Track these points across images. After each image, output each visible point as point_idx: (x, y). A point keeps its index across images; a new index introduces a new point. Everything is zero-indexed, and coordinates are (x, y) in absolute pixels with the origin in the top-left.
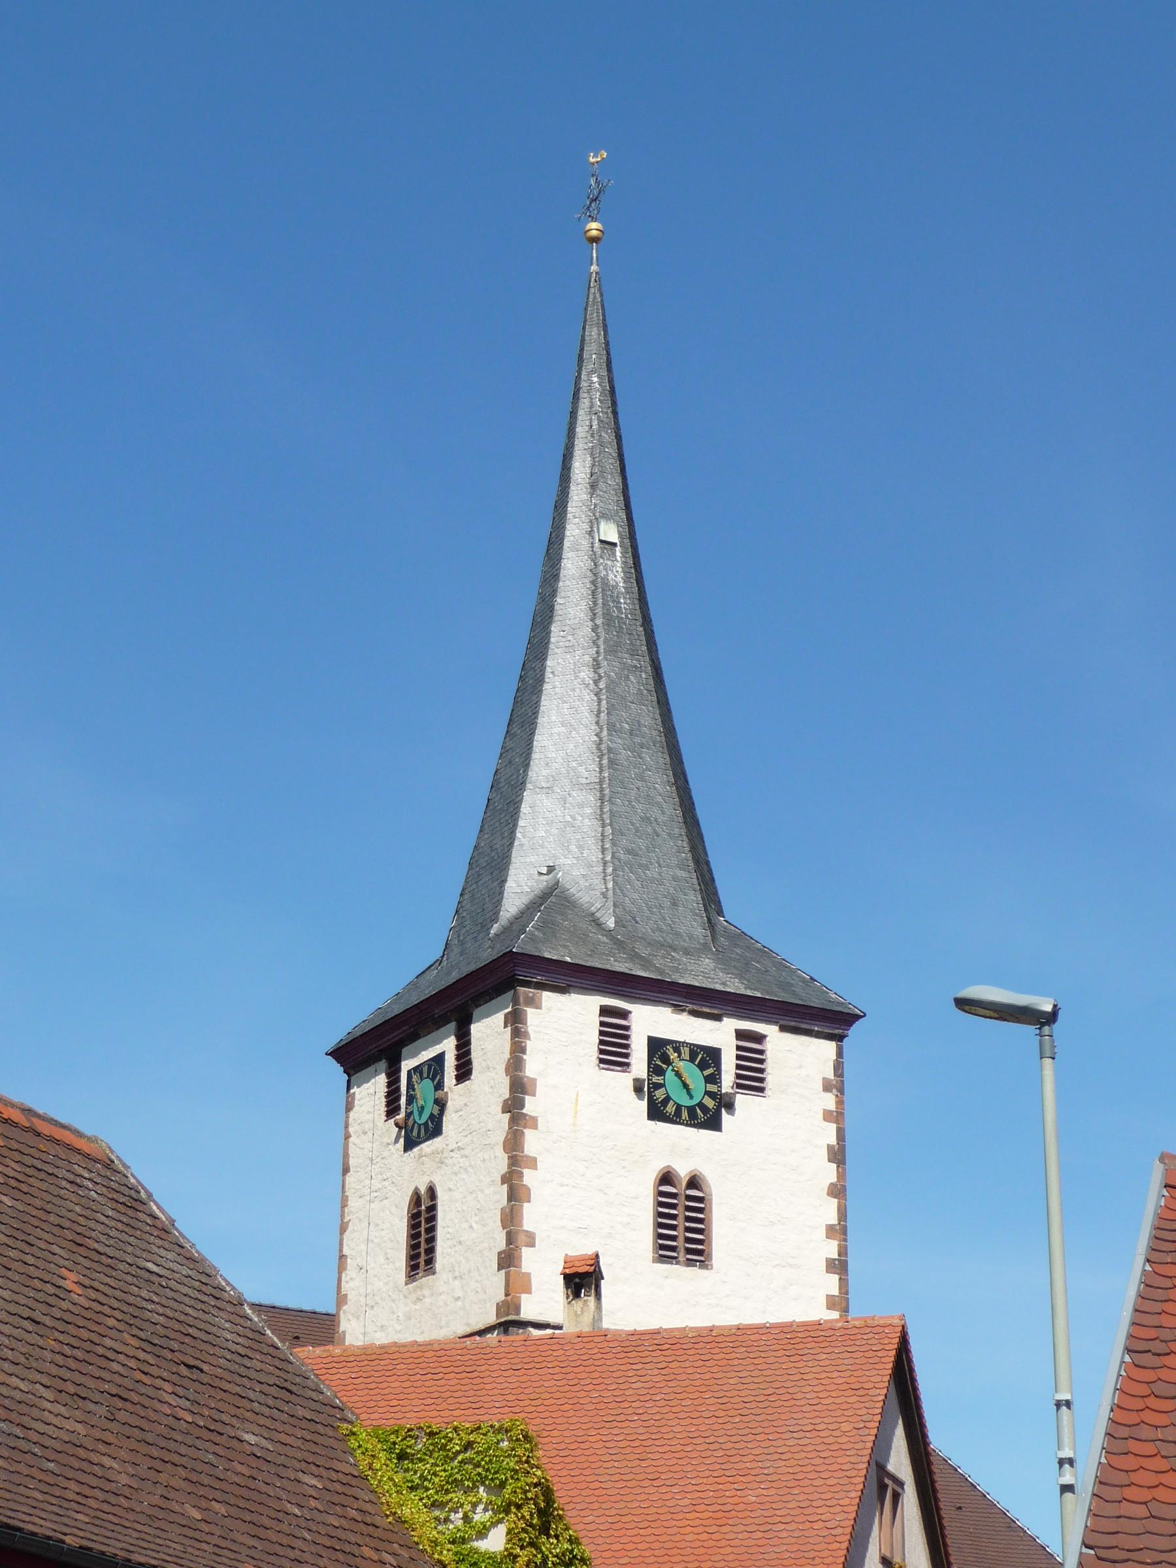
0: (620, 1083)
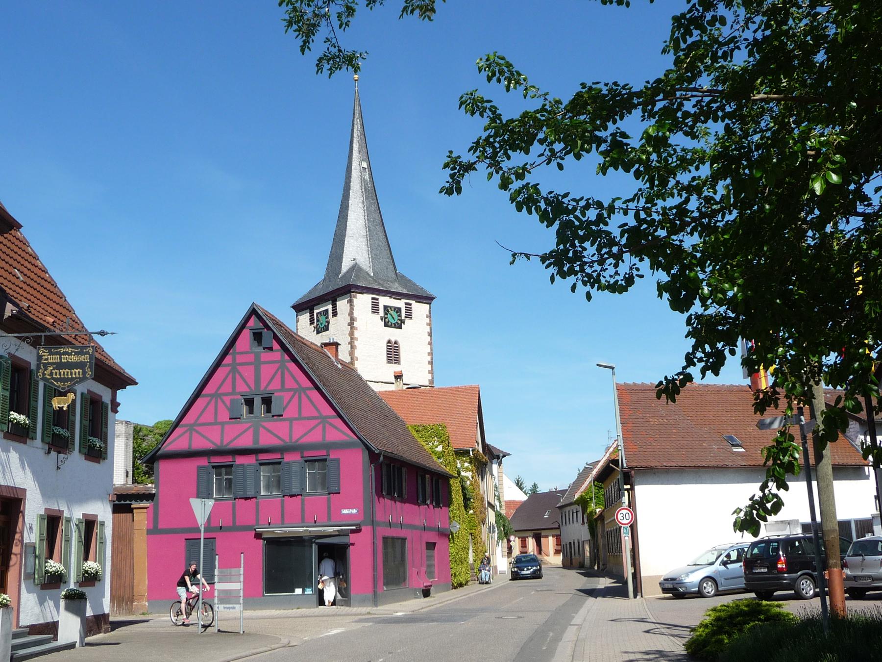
0: (377, 317)
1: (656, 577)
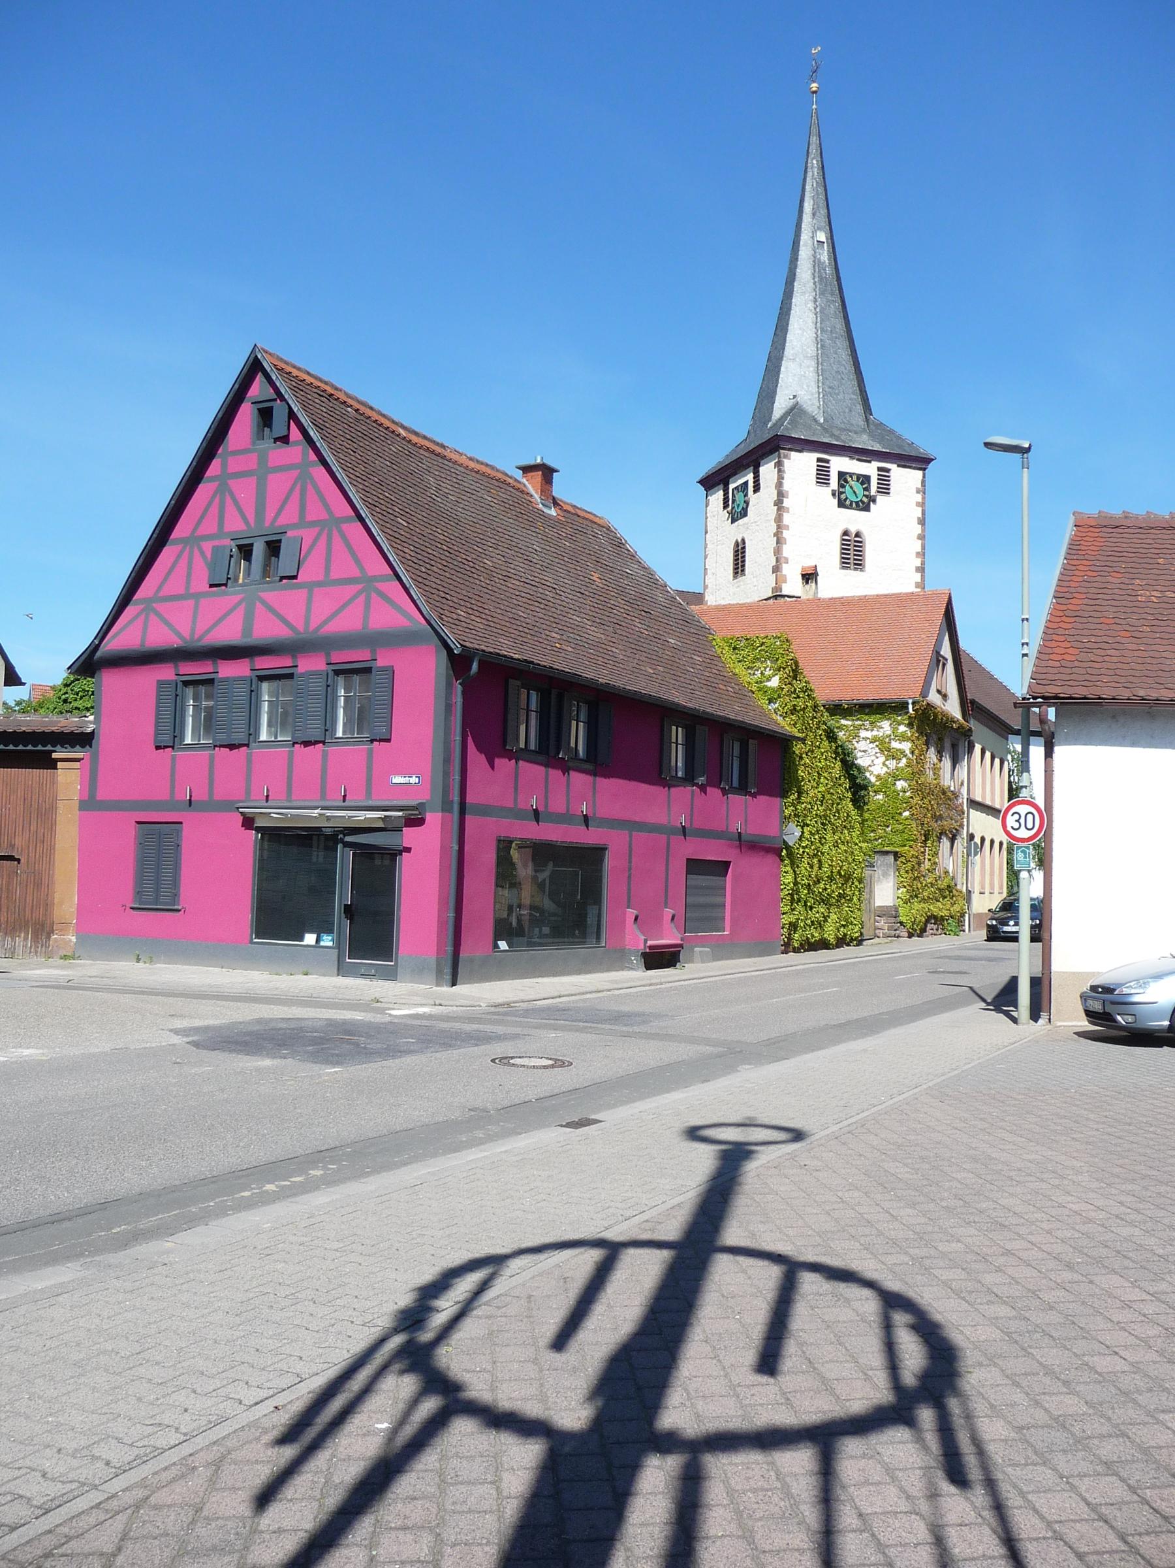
0: (826, 492)
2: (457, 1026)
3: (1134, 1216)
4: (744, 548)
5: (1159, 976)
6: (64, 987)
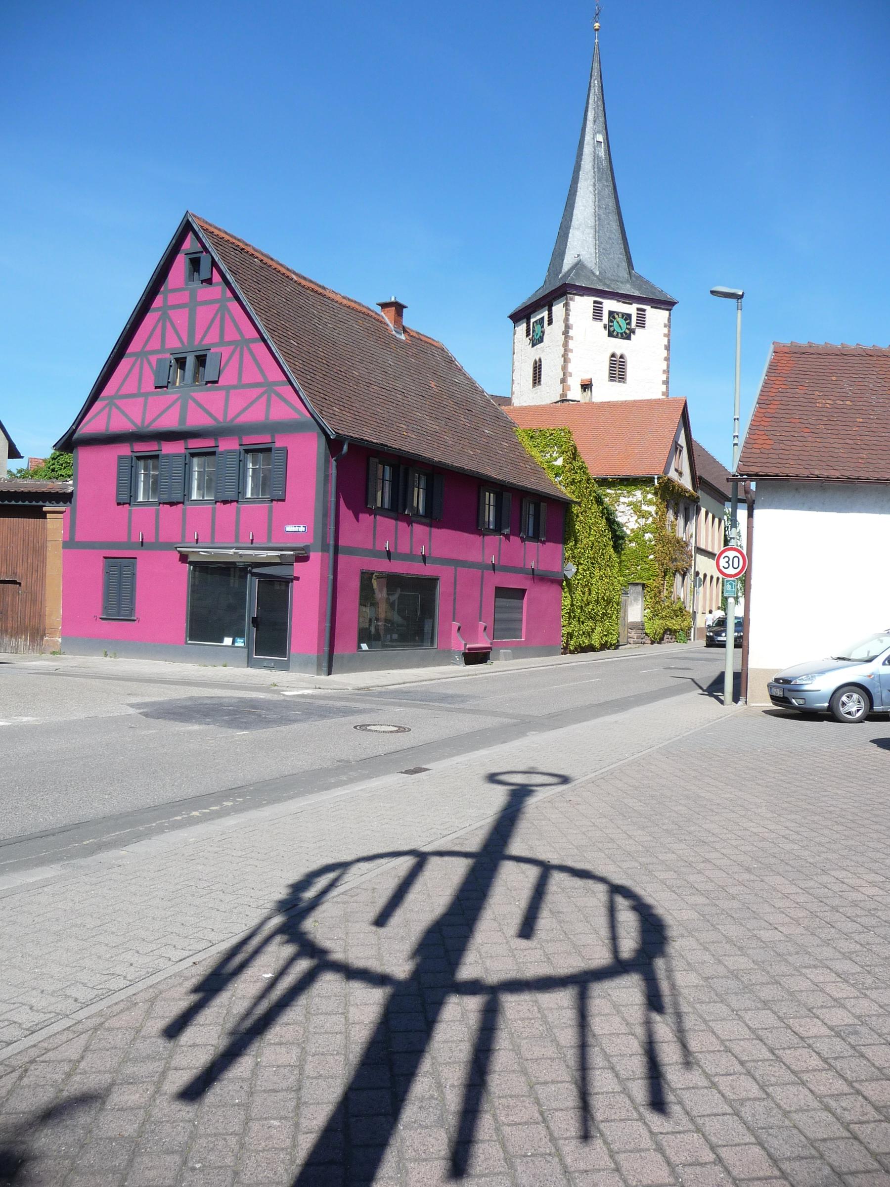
0: (599, 325)
1: (766, 671)
2: (331, 703)
3: (795, 837)
4: (540, 365)
5: (822, 672)
6: (53, 674)
